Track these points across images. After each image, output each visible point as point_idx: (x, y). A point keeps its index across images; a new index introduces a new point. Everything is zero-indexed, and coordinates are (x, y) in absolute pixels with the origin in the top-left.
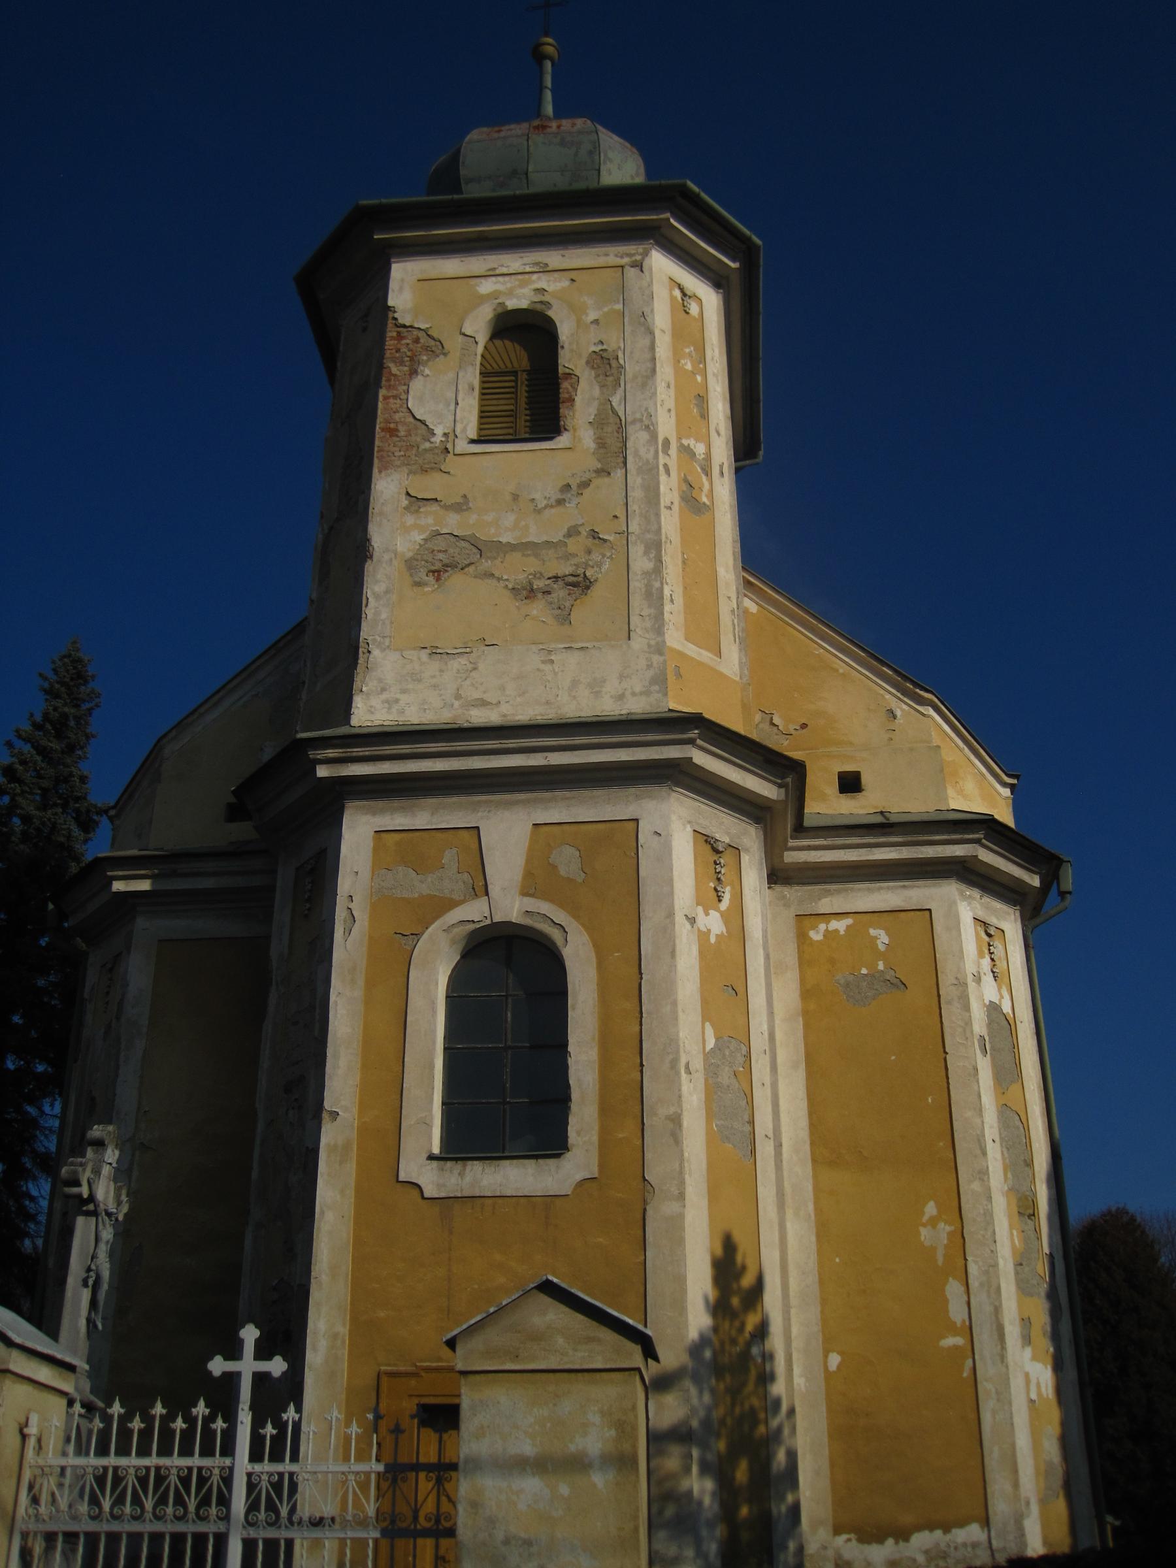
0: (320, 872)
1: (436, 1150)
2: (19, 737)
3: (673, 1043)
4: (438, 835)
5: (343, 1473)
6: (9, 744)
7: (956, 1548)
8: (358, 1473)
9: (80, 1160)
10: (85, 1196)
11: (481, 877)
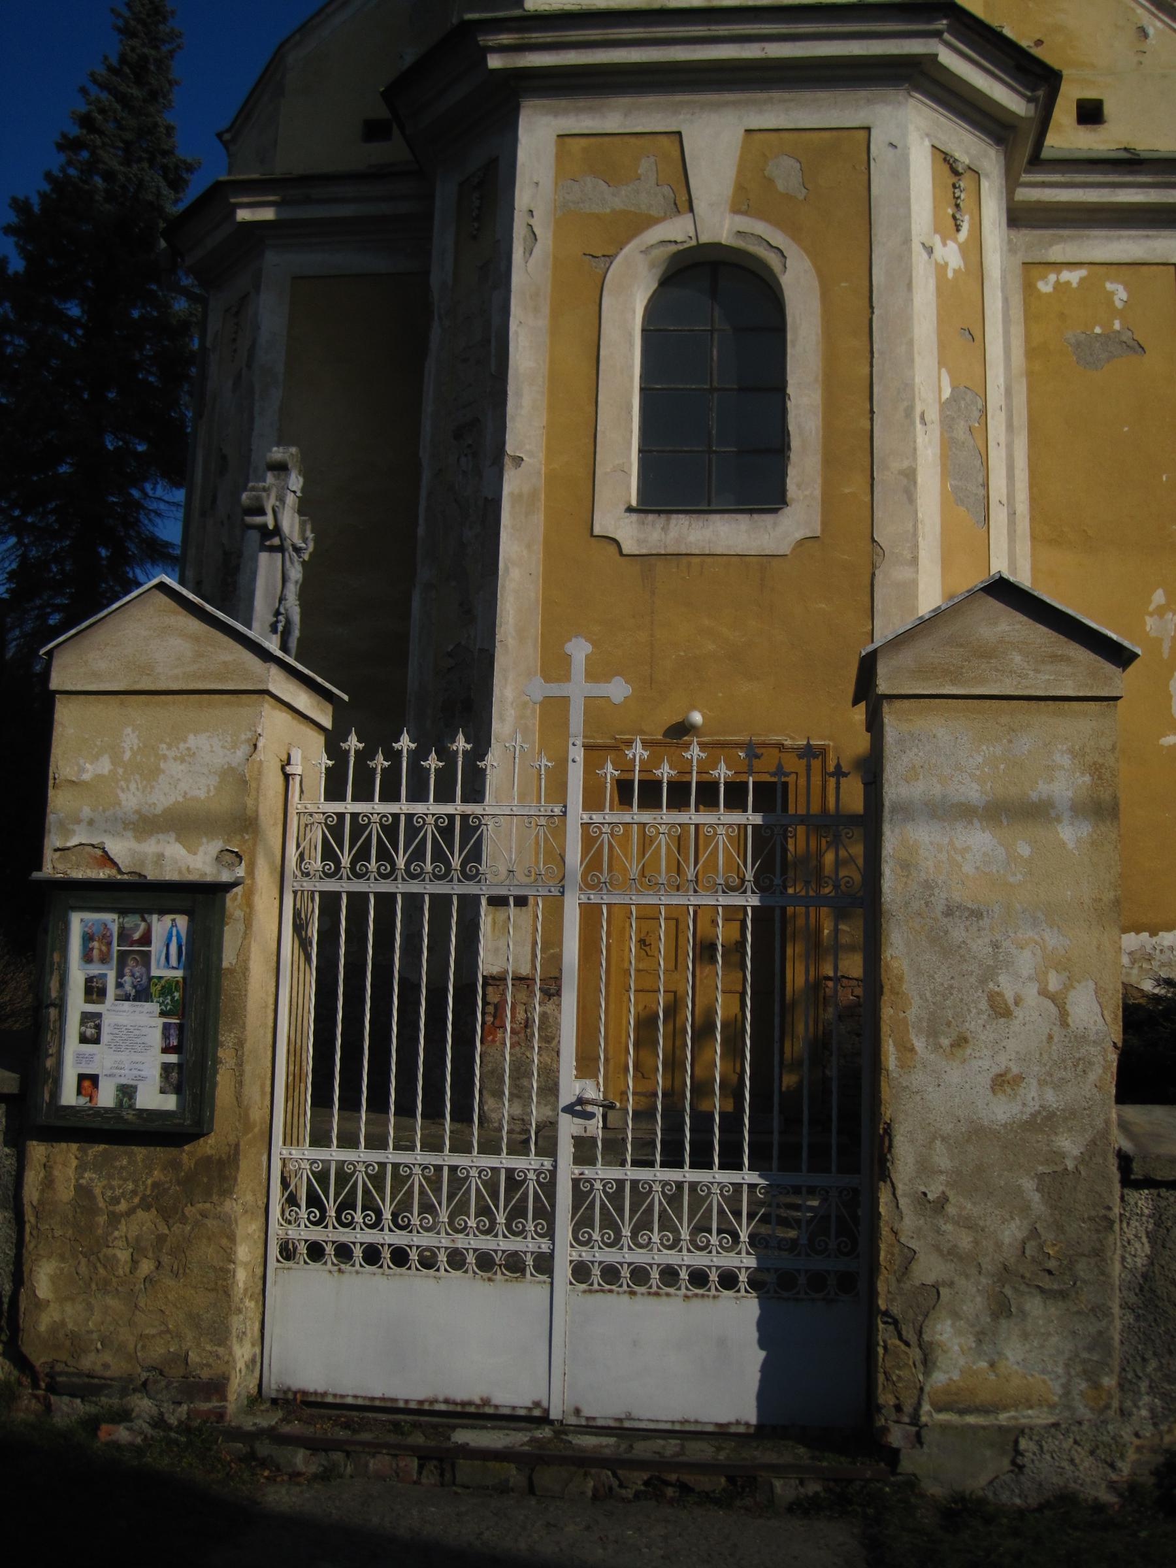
0: (492, 185)
1: (634, 503)
2: (95, 81)
3: (908, 387)
4: (633, 140)
5: (711, 825)
6: (83, 91)
7: (1161, 951)
8: (731, 825)
9: (261, 484)
10: (271, 527)
11: (685, 191)
